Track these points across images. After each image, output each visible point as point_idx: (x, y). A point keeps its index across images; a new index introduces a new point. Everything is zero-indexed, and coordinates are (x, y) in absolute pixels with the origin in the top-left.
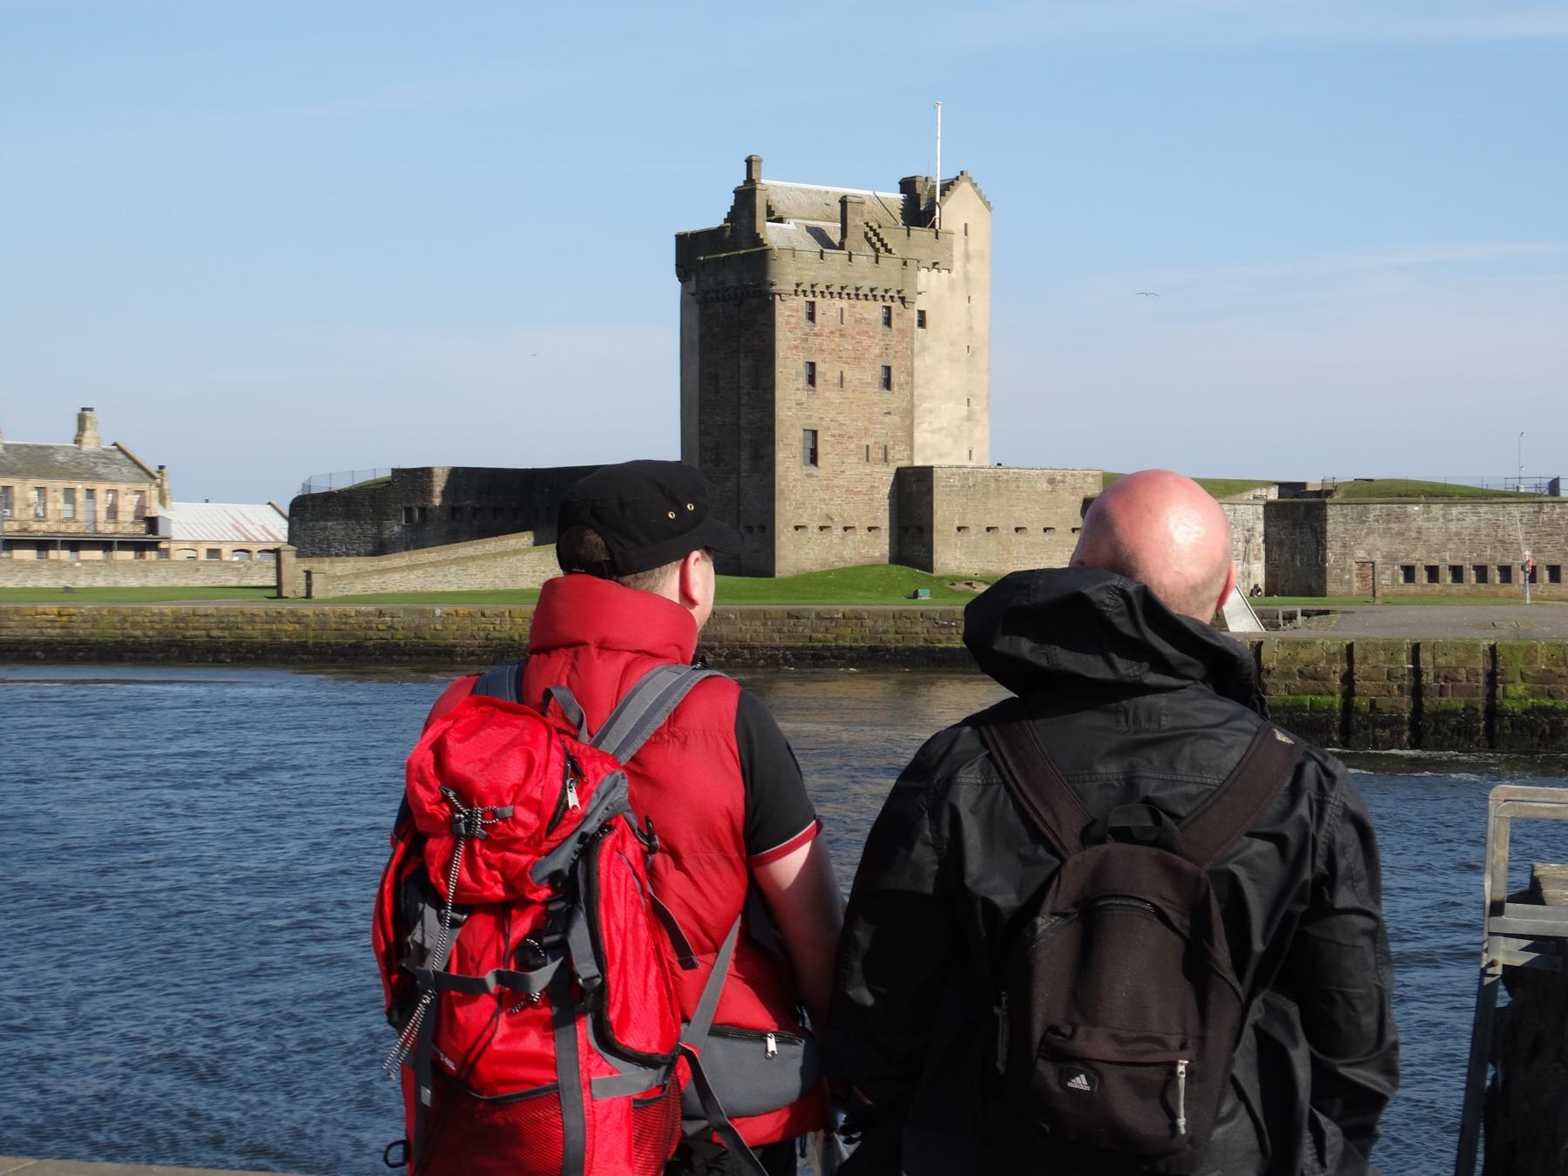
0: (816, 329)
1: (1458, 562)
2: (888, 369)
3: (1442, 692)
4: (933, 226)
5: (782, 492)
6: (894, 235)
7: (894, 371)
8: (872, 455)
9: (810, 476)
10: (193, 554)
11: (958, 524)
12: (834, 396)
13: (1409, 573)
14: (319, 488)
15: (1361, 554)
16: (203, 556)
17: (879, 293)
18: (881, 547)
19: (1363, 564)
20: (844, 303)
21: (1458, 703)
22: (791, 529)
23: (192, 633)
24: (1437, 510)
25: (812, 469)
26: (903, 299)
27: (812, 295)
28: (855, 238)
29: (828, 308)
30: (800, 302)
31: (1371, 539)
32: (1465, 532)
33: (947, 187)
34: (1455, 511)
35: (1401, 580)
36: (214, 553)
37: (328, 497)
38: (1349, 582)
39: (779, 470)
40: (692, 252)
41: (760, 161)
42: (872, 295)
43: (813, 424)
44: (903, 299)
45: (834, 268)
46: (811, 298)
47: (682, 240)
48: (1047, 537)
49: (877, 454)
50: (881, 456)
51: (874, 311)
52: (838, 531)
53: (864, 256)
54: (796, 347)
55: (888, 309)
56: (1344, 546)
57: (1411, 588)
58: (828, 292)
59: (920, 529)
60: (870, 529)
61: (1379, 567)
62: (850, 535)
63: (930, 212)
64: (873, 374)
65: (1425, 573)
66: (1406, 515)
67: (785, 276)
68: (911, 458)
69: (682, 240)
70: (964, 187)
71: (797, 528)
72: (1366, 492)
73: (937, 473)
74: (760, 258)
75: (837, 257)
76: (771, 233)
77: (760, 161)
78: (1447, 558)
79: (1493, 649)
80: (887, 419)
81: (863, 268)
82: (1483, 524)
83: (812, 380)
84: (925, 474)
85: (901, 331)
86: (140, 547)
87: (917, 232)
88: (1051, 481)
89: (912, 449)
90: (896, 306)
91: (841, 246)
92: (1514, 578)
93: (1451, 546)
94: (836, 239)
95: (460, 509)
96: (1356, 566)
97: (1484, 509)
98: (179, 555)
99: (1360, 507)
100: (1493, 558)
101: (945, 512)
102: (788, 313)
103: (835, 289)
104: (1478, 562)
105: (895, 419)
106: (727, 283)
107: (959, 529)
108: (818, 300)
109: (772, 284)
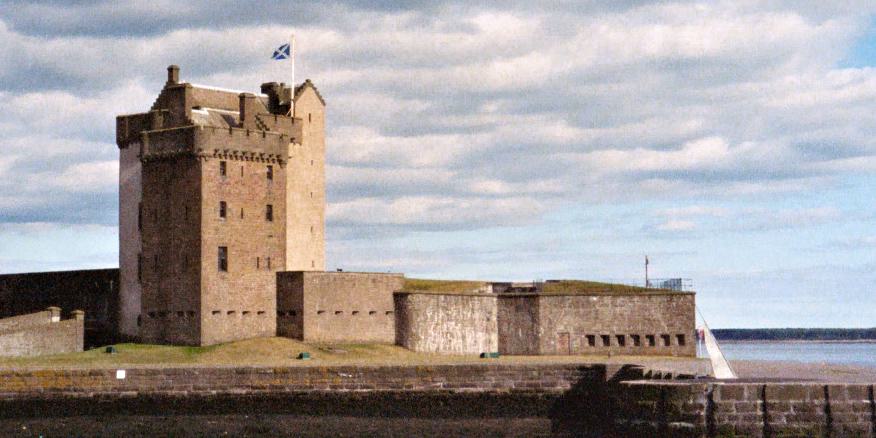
0: (228, 180)
2: (270, 207)
4: (290, 115)
5: (205, 288)
6: (269, 120)
7: (274, 209)
11: (318, 309)
12: (238, 224)
13: (591, 339)
15: (561, 328)
17: (239, 154)
18: (270, 323)
19: (562, 334)
20: (244, 163)
22: (211, 314)
23: (461, 390)
24: (607, 300)
25: (224, 273)
26: (280, 162)
27: (224, 155)
28: (250, 122)
29: (234, 166)
30: (216, 162)
31: (568, 318)
32: (625, 313)
33: (299, 90)
34: (620, 300)
35: (587, 344)
38: (554, 346)
41: (178, 69)
43: (225, 242)
44: (280, 162)
45: (238, 141)
47: (120, 120)
49: (263, 264)
50: (266, 264)
51: (261, 169)
52: (240, 315)
53: (256, 135)
54: (214, 192)
55: (270, 167)
56: (550, 322)
57: (592, 349)
58: (235, 156)
59: (293, 313)
60: (259, 313)
61: (573, 336)
62: (248, 318)
63: (287, 107)
64: (262, 210)
66: (588, 302)
67: (207, 146)
68: (284, 265)
69: (120, 120)
70: (309, 90)
71: (214, 313)
72: (562, 289)
73: (306, 276)
75: (239, 133)
76: (200, 117)
77: (178, 69)
78: (616, 329)
80: (271, 240)
81: (256, 143)
82: (636, 308)
83: (223, 213)
84: (297, 276)
85: (278, 183)
87: (280, 118)
88: (374, 281)
89: (285, 259)
90: (276, 166)
91: (241, 126)
92: (671, 341)
94: (237, 122)
96: (558, 336)
97: (636, 299)
99: (560, 298)
101: (311, 303)
102: (209, 168)
103: (239, 154)
104: (634, 332)
105: (274, 239)
106: (163, 149)
107: (319, 312)
108: (228, 161)
109: (200, 150)
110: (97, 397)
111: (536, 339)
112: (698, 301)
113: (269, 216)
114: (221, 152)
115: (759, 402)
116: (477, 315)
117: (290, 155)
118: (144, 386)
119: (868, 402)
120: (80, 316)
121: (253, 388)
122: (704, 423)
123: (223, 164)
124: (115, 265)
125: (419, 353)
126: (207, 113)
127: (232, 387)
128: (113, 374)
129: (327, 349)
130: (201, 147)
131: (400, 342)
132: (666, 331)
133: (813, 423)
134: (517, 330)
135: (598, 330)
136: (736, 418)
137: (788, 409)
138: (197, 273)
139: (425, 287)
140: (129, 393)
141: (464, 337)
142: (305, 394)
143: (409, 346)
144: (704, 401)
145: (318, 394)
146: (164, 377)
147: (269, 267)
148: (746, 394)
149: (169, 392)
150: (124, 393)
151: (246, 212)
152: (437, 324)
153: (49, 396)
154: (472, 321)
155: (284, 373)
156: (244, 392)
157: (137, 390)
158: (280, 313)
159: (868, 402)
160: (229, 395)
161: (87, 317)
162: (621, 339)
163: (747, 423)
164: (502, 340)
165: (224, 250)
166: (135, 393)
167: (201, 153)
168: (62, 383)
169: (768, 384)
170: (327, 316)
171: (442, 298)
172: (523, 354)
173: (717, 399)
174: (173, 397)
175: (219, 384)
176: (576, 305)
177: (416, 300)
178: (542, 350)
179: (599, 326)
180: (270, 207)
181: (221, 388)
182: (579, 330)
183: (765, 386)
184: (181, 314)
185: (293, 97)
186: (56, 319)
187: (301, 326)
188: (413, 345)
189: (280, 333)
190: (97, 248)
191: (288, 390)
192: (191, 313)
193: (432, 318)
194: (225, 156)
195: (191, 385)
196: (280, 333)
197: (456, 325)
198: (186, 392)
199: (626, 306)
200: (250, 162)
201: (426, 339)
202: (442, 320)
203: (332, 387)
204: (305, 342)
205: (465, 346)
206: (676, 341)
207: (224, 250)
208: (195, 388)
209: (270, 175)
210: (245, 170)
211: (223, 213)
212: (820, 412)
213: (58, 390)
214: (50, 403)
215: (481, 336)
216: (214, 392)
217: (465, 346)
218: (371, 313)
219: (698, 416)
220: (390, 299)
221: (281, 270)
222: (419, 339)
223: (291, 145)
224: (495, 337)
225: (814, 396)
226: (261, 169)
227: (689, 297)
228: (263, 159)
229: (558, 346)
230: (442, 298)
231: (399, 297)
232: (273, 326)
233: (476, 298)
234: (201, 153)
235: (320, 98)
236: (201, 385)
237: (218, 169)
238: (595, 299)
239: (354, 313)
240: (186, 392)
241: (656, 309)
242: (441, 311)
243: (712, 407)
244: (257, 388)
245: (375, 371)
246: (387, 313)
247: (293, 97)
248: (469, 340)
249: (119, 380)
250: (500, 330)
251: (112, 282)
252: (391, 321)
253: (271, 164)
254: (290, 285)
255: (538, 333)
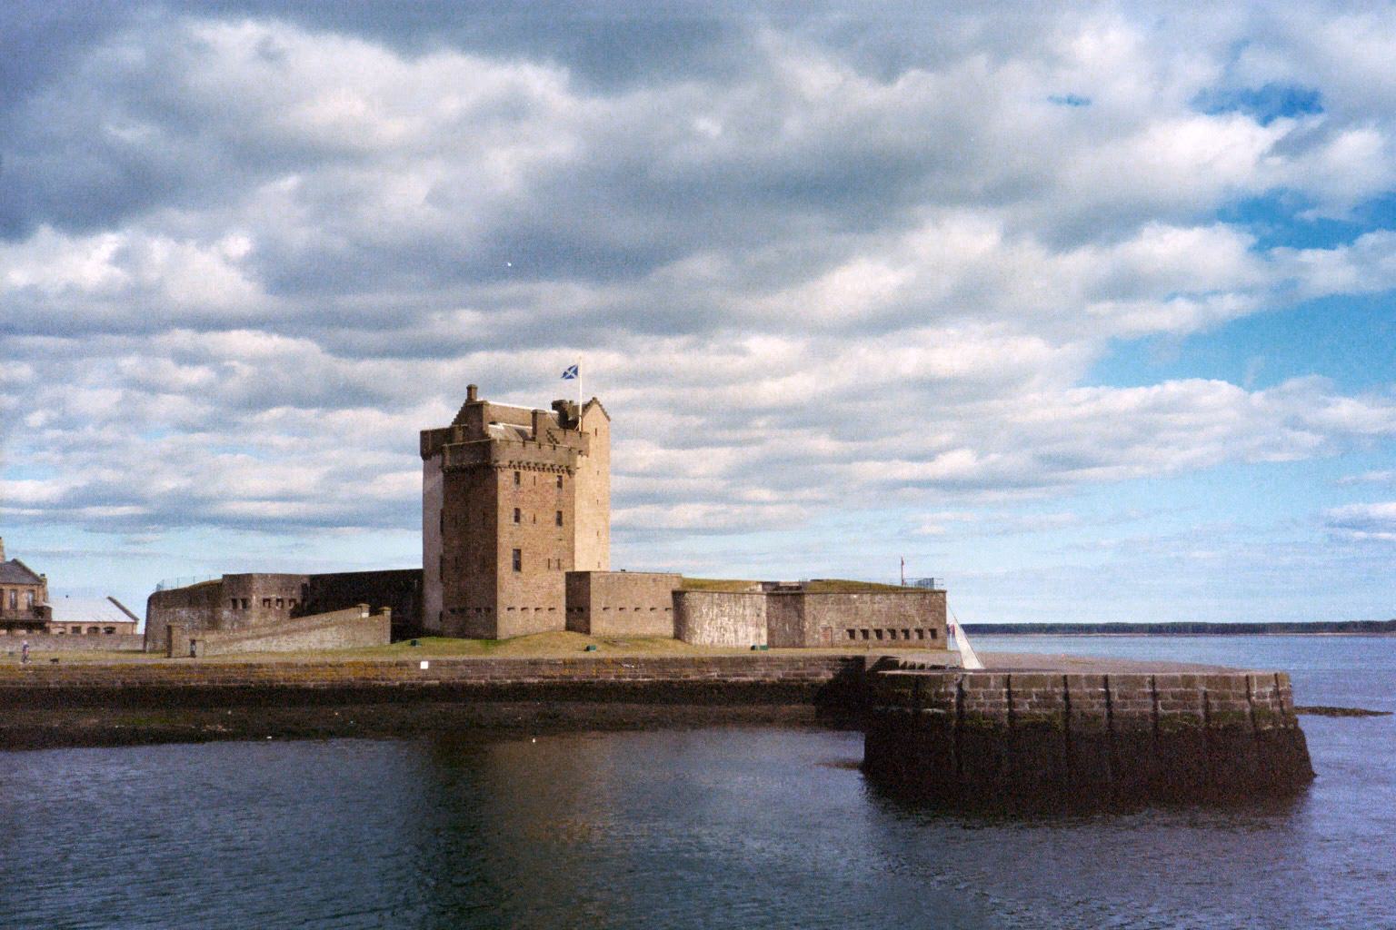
1: (879, 628)
2: (560, 513)
3: (1124, 705)
4: (578, 429)
6: (559, 435)
8: (552, 565)
9: (517, 578)
10: (63, 630)
11: (603, 606)
12: (530, 529)
13: (852, 633)
14: (168, 587)
15: (824, 623)
16: (69, 631)
18: (560, 618)
19: (825, 629)
20: (536, 474)
21: (1136, 711)
22: (506, 610)
24: (867, 597)
25: (517, 573)
27: (518, 466)
28: (542, 436)
30: (511, 472)
31: (830, 614)
32: (883, 610)
33: (586, 407)
34: (878, 598)
35: (848, 638)
36: (77, 630)
37: (176, 593)
39: (499, 573)
40: (433, 443)
41: (476, 388)
42: (552, 468)
43: (519, 545)
45: (531, 454)
46: (518, 470)
48: (652, 614)
49: (553, 565)
50: (556, 565)
51: (552, 479)
53: (547, 448)
55: (560, 477)
57: (853, 642)
58: (528, 467)
59: (581, 610)
61: (835, 630)
63: (575, 422)
64: (552, 516)
65: (861, 634)
68: (573, 566)
69: (424, 434)
70: (595, 407)
71: (509, 609)
73: (593, 575)
74: (485, 447)
75: (532, 446)
76: (496, 431)
77: (476, 388)
79: (1276, 675)
80: (560, 543)
81: (547, 455)
83: (517, 519)
84: (585, 576)
86: (29, 626)
87: (569, 432)
88: (654, 580)
89: (574, 561)
90: (565, 476)
91: (533, 439)
93: (875, 618)
95: (269, 600)
96: (821, 631)
98: (55, 631)
100: (898, 625)
101: (597, 601)
102: (505, 478)
103: (532, 465)
104: (890, 627)
105: (564, 543)
107: (604, 609)
108: (522, 471)
109: (497, 461)
110: (402, 685)
111: (802, 633)
112: (949, 598)
113: (559, 522)
114: (515, 463)
115: (1005, 690)
116: (748, 612)
117: (578, 466)
118: (445, 675)
119: (1103, 690)
120: (388, 612)
121: (544, 677)
122: (955, 709)
123: (517, 474)
124: (419, 566)
125: (696, 646)
126: (503, 428)
127: (525, 676)
128: (418, 664)
129: (611, 642)
130: (498, 458)
131: (678, 636)
132: (920, 626)
133: (1053, 709)
134: (784, 625)
135: (858, 624)
136: (983, 705)
137: (1031, 697)
138: (494, 573)
139: (701, 586)
140: (431, 682)
141: (736, 631)
142: (591, 683)
143: (687, 639)
144: (954, 690)
145: (604, 683)
146: (464, 667)
147: (559, 568)
148: (992, 683)
149: (469, 682)
150: (427, 682)
151: (539, 518)
152: (712, 620)
153: (359, 684)
154: (744, 617)
155: (573, 663)
156: (536, 681)
157: (439, 679)
158: (569, 610)
159: (1103, 690)
160: (523, 683)
161: (393, 613)
162: (879, 633)
163: (993, 710)
164: (771, 634)
165: (518, 552)
166: (437, 682)
167: (497, 464)
168: (371, 673)
169: (1012, 674)
170: (612, 612)
171: (716, 595)
172: (790, 646)
173: (966, 688)
174: (472, 686)
175: (513, 673)
176: (838, 602)
177: (693, 598)
178: (807, 643)
179: (859, 621)
180: (560, 513)
181: (515, 677)
182: (841, 625)
183: (1009, 676)
184: (479, 610)
185: (580, 413)
186: (365, 615)
187: (588, 622)
188: (690, 638)
189: (569, 628)
190: (403, 550)
191: (576, 679)
192: (488, 610)
193: (707, 614)
194: (519, 466)
195: (488, 675)
196: (569, 628)
197: (729, 620)
198: (483, 681)
199: (883, 603)
200: (542, 473)
201: (701, 633)
202: (717, 616)
203: (616, 677)
204: (591, 636)
205: (737, 640)
206: (929, 635)
207: (518, 552)
208: (491, 678)
209: (560, 485)
210: (537, 480)
211: (517, 519)
212: (1059, 699)
213: (368, 679)
214: (360, 691)
215: (752, 630)
216: (509, 681)
217: (737, 640)
218: (652, 609)
219: (949, 703)
220: (669, 597)
221: (570, 570)
222: (696, 633)
223: (579, 457)
224: (764, 631)
225: (1055, 685)
226: (552, 479)
227: (941, 595)
228: (553, 470)
229: (822, 640)
230: (716, 595)
231: (678, 595)
232: (563, 621)
233: (747, 596)
234: (497, 464)
235: (605, 414)
236: (497, 675)
237: (513, 479)
238: (855, 596)
239: (636, 609)
240: (483, 681)
241: (910, 605)
242: (715, 607)
243: (962, 695)
244: (548, 677)
245: (656, 662)
246: (666, 609)
247: (580, 413)
248: (741, 634)
249: (424, 670)
250: (769, 625)
251: (416, 581)
252: (669, 616)
253: (561, 474)
254: (578, 584)
255: (803, 627)
